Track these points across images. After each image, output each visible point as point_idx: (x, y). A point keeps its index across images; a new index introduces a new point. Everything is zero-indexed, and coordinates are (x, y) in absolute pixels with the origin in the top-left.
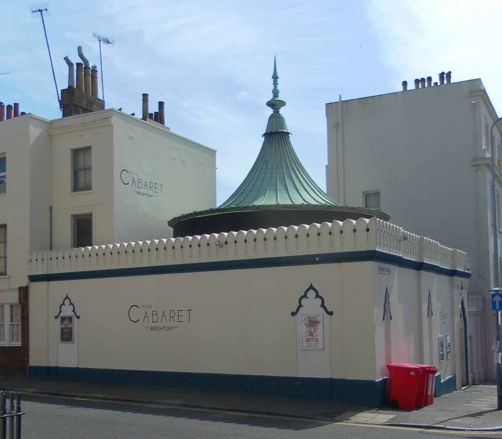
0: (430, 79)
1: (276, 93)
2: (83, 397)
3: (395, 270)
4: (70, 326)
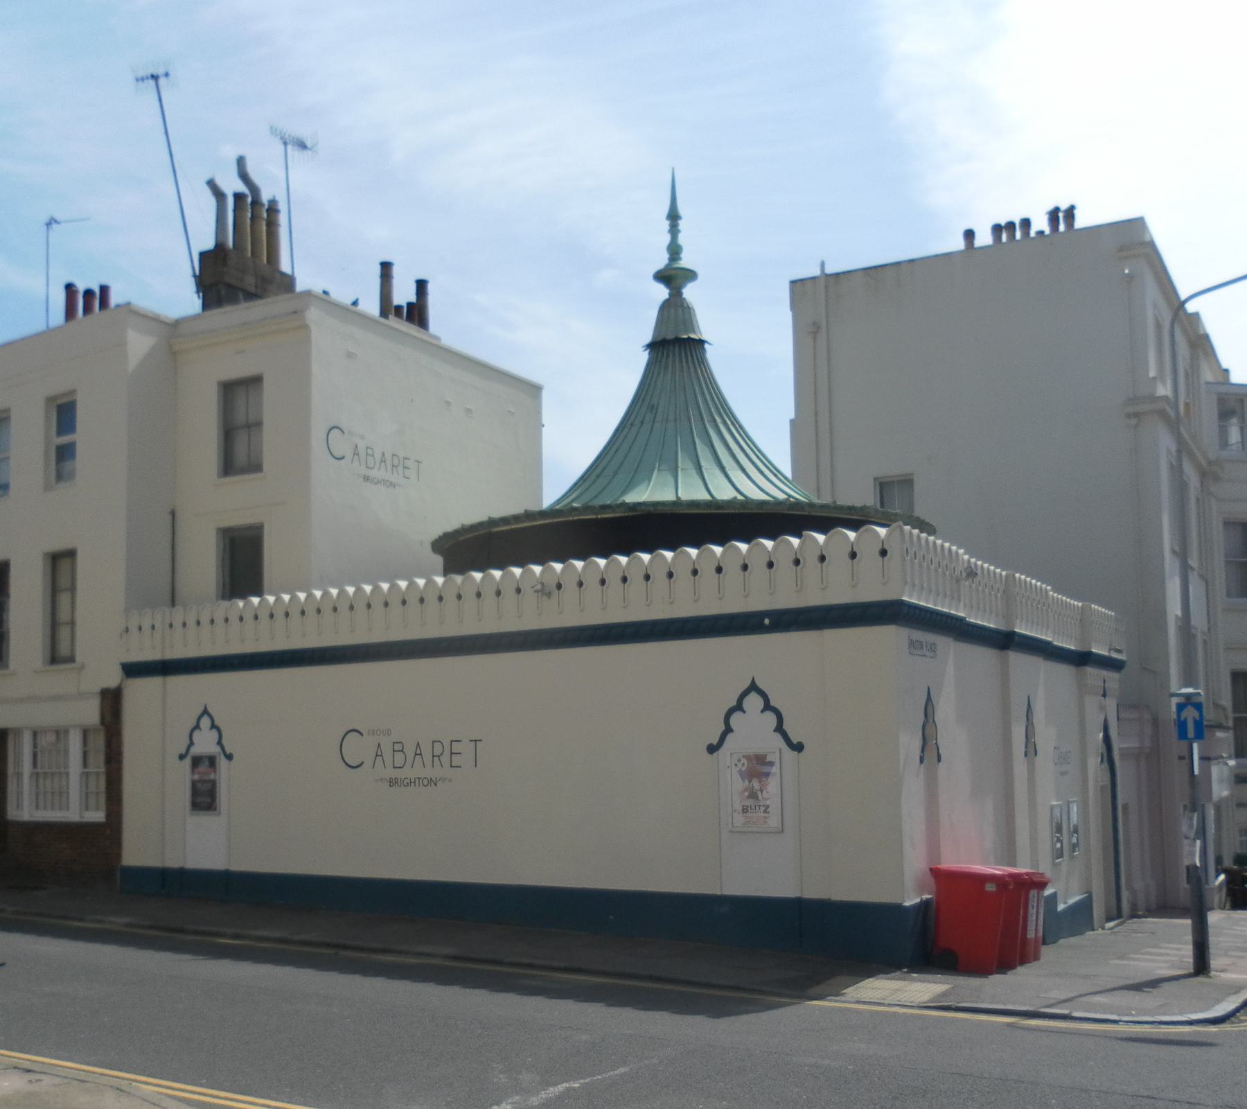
0: (1026, 223)
1: (674, 251)
2: (236, 936)
3: (949, 647)
4: (212, 776)
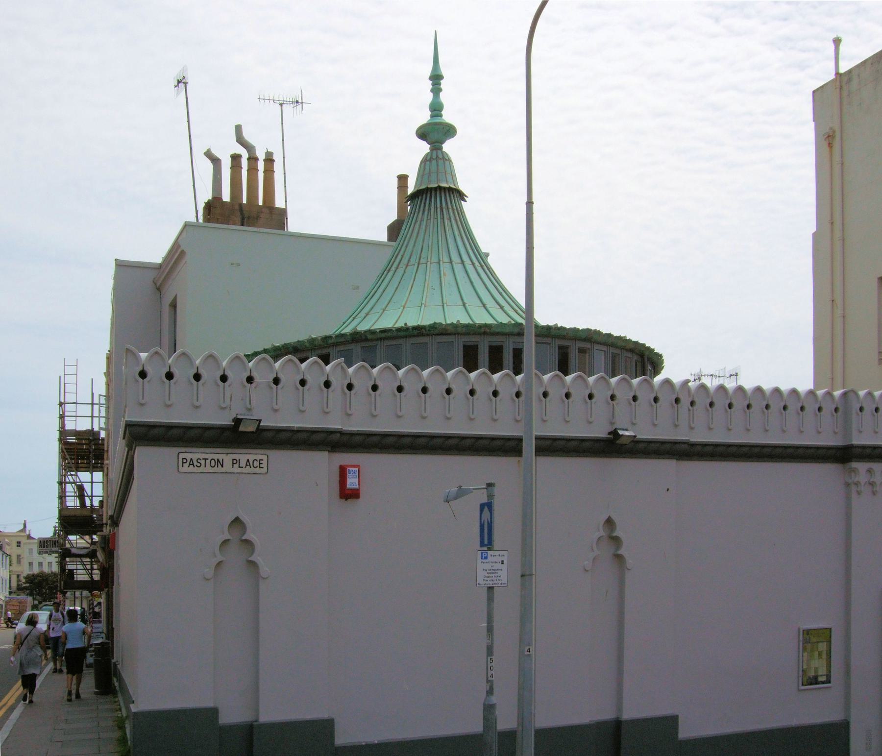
1: (436, 108)
